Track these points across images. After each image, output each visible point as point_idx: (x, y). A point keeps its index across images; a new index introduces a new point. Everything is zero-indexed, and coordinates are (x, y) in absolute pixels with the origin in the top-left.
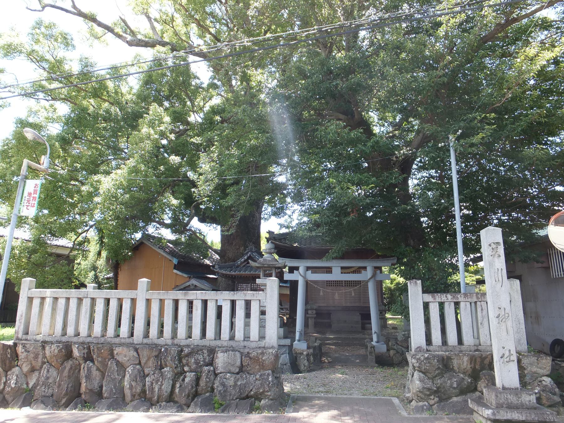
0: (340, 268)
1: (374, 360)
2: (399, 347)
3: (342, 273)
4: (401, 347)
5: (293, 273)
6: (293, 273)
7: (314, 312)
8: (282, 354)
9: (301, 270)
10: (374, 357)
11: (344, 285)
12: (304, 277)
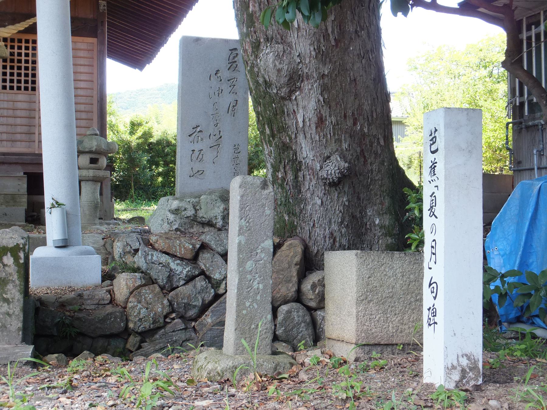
2: (157, 256)
4: (164, 258)
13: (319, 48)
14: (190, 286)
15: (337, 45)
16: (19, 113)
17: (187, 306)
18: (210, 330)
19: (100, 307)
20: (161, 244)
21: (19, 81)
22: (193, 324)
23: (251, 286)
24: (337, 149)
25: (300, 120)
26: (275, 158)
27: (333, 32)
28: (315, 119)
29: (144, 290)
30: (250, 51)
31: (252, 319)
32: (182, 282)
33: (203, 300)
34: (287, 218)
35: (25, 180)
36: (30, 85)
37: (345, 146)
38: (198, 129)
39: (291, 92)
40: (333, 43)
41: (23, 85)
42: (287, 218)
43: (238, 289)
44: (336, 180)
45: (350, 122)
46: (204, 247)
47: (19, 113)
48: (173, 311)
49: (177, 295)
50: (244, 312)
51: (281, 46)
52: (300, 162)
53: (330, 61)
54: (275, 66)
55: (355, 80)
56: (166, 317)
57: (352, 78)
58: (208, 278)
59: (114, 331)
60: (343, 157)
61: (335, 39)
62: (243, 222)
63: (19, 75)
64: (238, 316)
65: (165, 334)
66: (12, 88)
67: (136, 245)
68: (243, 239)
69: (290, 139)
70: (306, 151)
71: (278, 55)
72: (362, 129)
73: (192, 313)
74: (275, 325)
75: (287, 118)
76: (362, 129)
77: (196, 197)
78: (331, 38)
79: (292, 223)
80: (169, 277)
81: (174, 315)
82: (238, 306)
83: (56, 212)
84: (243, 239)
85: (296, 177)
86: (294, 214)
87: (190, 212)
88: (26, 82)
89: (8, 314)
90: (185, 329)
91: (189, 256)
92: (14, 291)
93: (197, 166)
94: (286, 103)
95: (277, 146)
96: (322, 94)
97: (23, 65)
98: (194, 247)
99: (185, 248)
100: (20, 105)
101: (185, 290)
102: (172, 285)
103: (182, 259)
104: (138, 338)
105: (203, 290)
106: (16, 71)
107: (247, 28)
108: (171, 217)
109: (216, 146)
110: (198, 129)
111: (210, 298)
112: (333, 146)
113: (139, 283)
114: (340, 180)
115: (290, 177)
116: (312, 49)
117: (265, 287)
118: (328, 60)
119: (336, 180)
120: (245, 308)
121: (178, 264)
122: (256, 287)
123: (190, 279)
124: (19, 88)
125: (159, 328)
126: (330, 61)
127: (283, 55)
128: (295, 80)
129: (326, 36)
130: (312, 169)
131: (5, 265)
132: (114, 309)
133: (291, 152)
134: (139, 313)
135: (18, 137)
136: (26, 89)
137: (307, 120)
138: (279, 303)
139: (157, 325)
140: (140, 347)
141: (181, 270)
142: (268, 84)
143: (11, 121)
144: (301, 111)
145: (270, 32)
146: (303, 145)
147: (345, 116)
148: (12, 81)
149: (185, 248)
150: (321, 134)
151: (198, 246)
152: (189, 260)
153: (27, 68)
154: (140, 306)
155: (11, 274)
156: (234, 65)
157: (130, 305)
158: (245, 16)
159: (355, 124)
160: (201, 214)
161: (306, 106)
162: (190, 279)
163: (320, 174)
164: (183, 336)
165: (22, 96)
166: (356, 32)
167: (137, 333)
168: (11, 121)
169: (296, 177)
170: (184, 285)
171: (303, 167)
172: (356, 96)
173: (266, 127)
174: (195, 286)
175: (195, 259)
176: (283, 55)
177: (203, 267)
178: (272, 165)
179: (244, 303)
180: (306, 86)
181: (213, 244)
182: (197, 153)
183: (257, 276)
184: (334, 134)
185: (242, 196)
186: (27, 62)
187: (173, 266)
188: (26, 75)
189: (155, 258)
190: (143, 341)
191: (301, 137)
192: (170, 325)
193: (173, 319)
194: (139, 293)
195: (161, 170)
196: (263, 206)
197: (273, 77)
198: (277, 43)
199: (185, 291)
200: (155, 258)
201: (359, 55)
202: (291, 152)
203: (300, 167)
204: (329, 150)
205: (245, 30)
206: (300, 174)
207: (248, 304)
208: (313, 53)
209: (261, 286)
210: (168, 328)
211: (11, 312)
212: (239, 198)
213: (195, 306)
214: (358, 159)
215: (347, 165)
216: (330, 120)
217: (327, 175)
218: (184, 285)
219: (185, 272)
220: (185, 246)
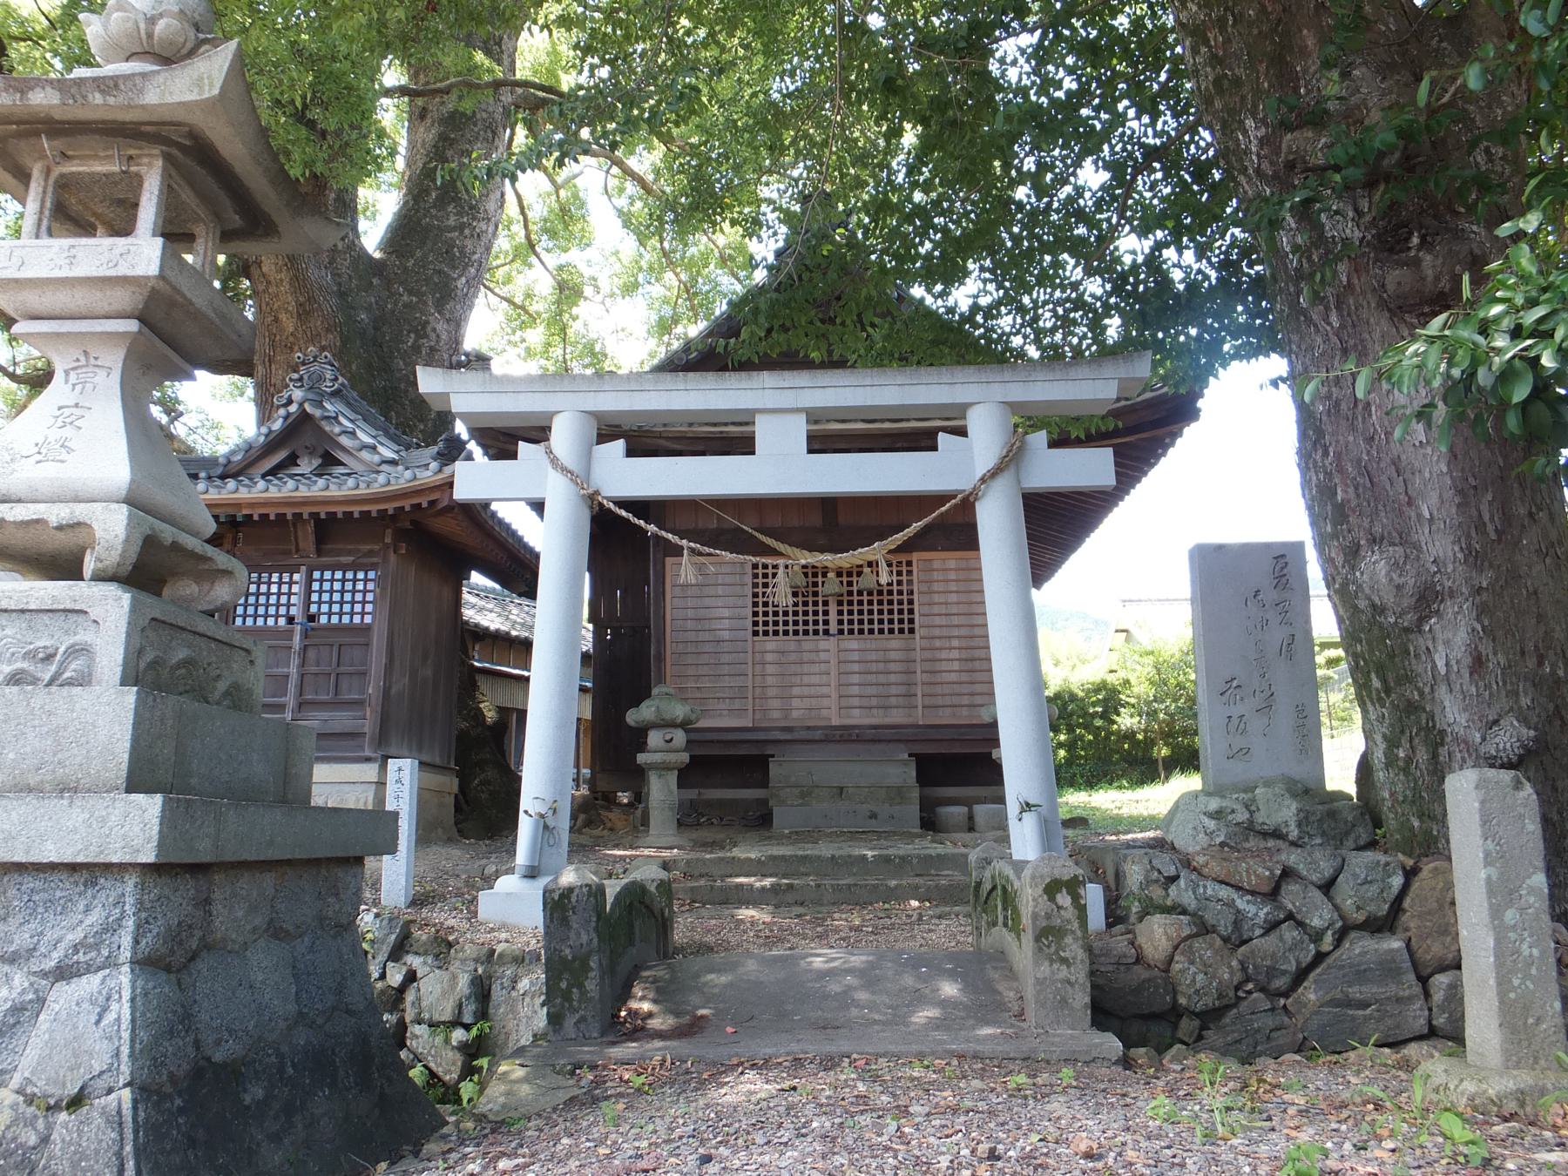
0: (803, 417)
1: (1081, 999)
2: (1211, 889)
3: (810, 451)
4: (1225, 892)
5: (513, 455)
6: (513, 455)
7: (680, 737)
8: (64, 973)
9: (563, 436)
10: (1080, 973)
11: (833, 627)
12: (578, 477)
13: (1469, 546)
14: (1272, 938)
15: (1499, 540)
16: (893, 667)
17: (1272, 972)
18: (1316, 1013)
19: (1122, 968)
20: (1215, 868)
21: (891, 621)
22: (1282, 1001)
23: (1518, 952)
24: (1511, 709)
25: (1441, 664)
26: (1391, 725)
27: (1492, 519)
28: (1468, 661)
29: (1197, 944)
30: (1340, 560)
31: (1526, 1009)
32: (1258, 932)
33: (1298, 963)
34: (1416, 824)
35: (913, 765)
36: (906, 626)
37: (1525, 701)
38: (1235, 684)
39: (1422, 620)
40: (1493, 536)
41: (866, 627)
42: (1416, 824)
43: (1496, 956)
44: (1514, 759)
45: (1531, 662)
46: (1288, 873)
47: (893, 667)
48: (1248, 980)
49: (1252, 952)
50: (1512, 995)
51: (1400, 550)
52: (1442, 733)
53: (1491, 566)
54: (1391, 580)
55: (1535, 593)
56: (1237, 988)
57: (1531, 589)
58: (1300, 924)
59: (1155, 1009)
60: (1524, 720)
61: (1496, 530)
62: (1490, 845)
63: (891, 612)
64: (1502, 1002)
65: (1240, 1016)
66: (881, 631)
67: (1172, 871)
68: (1493, 872)
69: (1421, 693)
70: (1453, 713)
71: (1396, 563)
72: (1553, 672)
73: (1280, 983)
74: (1430, 1010)
75: (1414, 662)
76: (1553, 672)
77: (1245, 791)
78: (1490, 528)
79: (1428, 833)
80: (1235, 922)
81: (1250, 986)
82: (1499, 984)
83: (1030, 818)
84: (1493, 872)
85: (1435, 756)
86: (1432, 818)
87: (1242, 816)
88: (901, 621)
89: (1069, 982)
90: (1273, 1009)
91: (1266, 889)
92: (1074, 947)
93: (1239, 742)
94: (1412, 637)
95: (1395, 707)
96: (1478, 619)
97: (895, 597)
98: (1272, 873)
99: (1257, 876)
100: (893, 655)
101: (1265, 945)
102: (1241, 935)
103: (1252, 893)
104: (1197, 1023)
105: (1294, 946)
106: (886, 607)
107: (1334, 525)
108: (1211, 824)
109: (1267, 707)
110: (1235, 684)
111: (1309, 959)
112: (1504, 703)
113: (1186, 932)
114: (1521, 759)
115: (1422, 755)
116: (1457, 548)
117: (1543, 952)
118: (1486, 564)
119: (1514, 759)
120: (1514, 989)
121: (1248, 902)
122: (1526, 953)
123: (1271, 927)
124: (891, 631)
125: (1228, 1007)
126: (1491, 566)
127: (1405, 563)
128: (1427, 600)
129: (1480, 527)
130: (1466, 742)
131: (1059, 908)
132: (1145, 974)
133: (1424, 716)
134: (1194, 980)
135: (893, 701)
136: (901, 631)
137: (1453, 662)
138: (1429, 970)
139: (1225, 1001)
140: (1200, 1038)
141: (1258, 912)
142: (1378, 610)
143: (882, 678)
144: (1440, 648)
145: (1378, 529)
146: (1447, 703)
147: (1523, 653)
148: (871, 622)
149: (1257, 876)
150: (1481, 684)
151: (1278, 872)
152: (1264, 895)
153: (900, 602)
154: (1193, 969)
155: (1069, 921)
156: (1284, 580)
157: (1176, 967)
158: (1329, 508)
159: (1540, 664)
160: (1260, 818)
161: (1450, 640)
162: (1271, 927)
163: (1482, 750)
164: (1270, 1021)
165: (895, 642)
166: (1531, 515)
167: (1193, 1013)
168: (882, 678)
169: (1435, 756)
170: (1262, 935)
171: (1448, 739)
172: (1540, 618)
173: (1373, 676)
174: (1281, 939)
175: (1273, 894)
176: (1405, 563)
177: (1290, 906)
178: (1384, 736)
179: (1510, 981)
180: (1449, 608)
181: (1302, 868)
182: (1235, 721)
183: (1526, 934)
184: (1505, 683)
185: (1483, 802)
186: (900, 593)
187: (1241, 903)
188: (901, 612)
189: (1209, 892)
190: (1203, 1027)
191: (1442, 690)
192: (1245, 1003)
193: (1250, 992)
194: (1190, 947)
195: (1062, 737)
196: (1521, 816)
197: (1389, 598)
198: (1393, 544)
199: (1265, 945)
200: (1209, 892)
201: (1539, 551)
202: (1424, 716)
203: (1442, 739)
204: (1497, 707)
205: (1329, 529)
206: (1443, 751)
207: (1516, 982)
208: (1460, 555)
209: (1535, 952)
210: (1243, 1006)
211: (1073, 979)
212: (1477, 805)
213: (1284, 972)
214: (1550, 722)
215: (1532, 733)
216: (1497, 661)
217: (1498, 751)
218: (1262, 935)
219: (1262, 914)
220: (1259, 872)
